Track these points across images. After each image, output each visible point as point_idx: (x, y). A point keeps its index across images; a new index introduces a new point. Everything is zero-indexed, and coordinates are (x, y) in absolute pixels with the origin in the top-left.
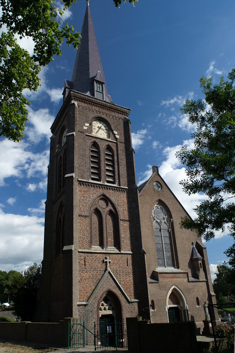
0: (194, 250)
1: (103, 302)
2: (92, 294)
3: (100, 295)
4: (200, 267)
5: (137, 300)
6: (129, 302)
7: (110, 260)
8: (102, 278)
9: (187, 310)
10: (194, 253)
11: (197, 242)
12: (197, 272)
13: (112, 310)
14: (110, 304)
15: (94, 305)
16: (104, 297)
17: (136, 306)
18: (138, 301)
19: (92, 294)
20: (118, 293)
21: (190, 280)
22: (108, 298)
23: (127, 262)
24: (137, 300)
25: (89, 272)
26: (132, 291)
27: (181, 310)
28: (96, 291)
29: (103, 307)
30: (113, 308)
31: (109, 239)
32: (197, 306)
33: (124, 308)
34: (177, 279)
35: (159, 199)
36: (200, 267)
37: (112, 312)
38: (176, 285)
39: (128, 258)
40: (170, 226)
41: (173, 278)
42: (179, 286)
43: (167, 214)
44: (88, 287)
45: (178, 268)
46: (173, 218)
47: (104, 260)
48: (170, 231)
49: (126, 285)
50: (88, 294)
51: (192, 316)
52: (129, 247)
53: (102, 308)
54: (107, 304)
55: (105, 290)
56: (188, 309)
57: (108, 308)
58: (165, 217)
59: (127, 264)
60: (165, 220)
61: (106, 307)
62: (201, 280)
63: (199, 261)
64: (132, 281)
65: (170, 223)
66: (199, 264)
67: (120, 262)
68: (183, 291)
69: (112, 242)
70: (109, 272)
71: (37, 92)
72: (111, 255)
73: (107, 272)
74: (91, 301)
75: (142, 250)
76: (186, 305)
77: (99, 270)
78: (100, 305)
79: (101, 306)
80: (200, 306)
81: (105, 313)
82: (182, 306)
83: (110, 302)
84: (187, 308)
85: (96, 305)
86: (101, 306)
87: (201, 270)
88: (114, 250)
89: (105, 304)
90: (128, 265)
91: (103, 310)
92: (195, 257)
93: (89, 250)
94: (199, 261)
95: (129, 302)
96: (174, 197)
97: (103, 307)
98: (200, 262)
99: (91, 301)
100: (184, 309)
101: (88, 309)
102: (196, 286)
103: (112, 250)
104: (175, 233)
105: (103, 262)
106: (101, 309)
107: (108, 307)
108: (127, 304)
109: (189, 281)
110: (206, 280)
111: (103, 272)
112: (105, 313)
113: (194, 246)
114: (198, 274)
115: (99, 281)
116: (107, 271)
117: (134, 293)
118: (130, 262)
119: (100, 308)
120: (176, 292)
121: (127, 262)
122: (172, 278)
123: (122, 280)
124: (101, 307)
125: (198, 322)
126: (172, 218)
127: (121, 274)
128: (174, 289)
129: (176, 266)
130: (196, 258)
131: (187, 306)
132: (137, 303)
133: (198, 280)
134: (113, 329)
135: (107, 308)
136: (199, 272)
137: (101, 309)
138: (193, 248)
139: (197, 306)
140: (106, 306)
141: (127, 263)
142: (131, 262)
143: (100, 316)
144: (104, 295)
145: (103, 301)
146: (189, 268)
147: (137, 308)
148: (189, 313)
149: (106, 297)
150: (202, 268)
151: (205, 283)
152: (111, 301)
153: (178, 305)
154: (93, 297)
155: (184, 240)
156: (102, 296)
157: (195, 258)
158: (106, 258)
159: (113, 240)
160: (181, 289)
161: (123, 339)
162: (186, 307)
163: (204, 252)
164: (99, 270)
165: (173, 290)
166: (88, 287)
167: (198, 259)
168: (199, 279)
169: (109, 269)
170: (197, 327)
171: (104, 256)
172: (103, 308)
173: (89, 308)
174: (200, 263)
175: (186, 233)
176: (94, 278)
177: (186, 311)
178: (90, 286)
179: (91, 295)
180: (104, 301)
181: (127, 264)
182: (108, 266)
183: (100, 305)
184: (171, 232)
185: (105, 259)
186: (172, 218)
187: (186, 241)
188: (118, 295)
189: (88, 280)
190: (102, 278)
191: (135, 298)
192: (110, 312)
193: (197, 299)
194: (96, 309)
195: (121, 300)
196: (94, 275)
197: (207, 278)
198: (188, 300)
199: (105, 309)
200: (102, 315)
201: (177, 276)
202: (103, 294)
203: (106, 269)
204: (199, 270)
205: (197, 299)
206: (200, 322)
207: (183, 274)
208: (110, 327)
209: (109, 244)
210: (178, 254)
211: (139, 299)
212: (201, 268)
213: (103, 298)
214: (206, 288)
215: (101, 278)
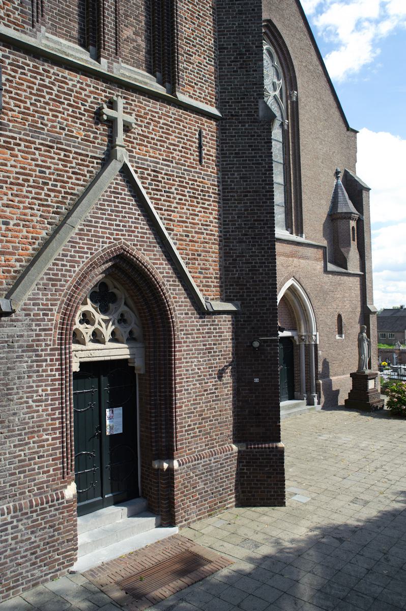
0: (340, 192)
1: (89, 307)
2: (32, 263)
3: (77, 269)
4: (351, 239)
5: (230, 307)
6: (202, 312)
7: (131, 119)
8: (91, 192)
9: (316, 345)
10: (340, 199)
11: (346, 173)
12: (342, 250)
13: (131, 339)
14: (122, 315)
15: (47, 315)
16: (94, 282)
17: (225, 325)
18: (234, 309)
19: (32, 263)
20: (161, 271)
21: (329, 269)
22: (112, 290)
23: (200, 147)
24: (230, 307)
25: (22, 148)
26: (213, 269)
27: (299, 345)
28: (57, 249)
29: (91, 329)
30: (131, 333)
31: (127, 33)
32: (338, 337)
33: (180, 335)
34: (302, 261)
35: (269, 18)
36: (351, 239)
37: (127, 351)
38: (297, 277)
39: (204, 133)
40: (289, 111)
41: (292, 257)
42: (304, 282)
43: (281, 75)
44: (11, 226)
45: (300, 232)
46: (299, 90)
47: (101, 109)
48: (286, 127)
49: (191, 241)
50: (13, 262)
51: (325, 360)
52: (209, 89)
53: (86, 331)
54: (107, 318)
55: (101, 248)
56: (318, 343)
57: (113, 333)
58: (277, 82)
59: (200, 156)
60: (277, 93)
61: (103, 330)
62: (352, 272)
63: (351, 221)
64: (214, 229)
65: (289, 101)
66: (351, 228)
67: (173, 139)
68: (311, 295)
69: (137, 49)
70: (125, 171)
71: (79, 312)
72: (134, 97)
73: (114, 167)
74: (29, 293)
75: (261, 106)
76: (314, 333)
77: (73, 150)
78: (77, 320)
79: (81, 322)
80: (343, 335)
81: (97, 353)
82: (304, 334)
83: (123, 308)
84: (316, 340)
85: (57, 317)
86: (81, 322)
87: (354, 245)
88: (148, 81)
89: (99, 317)
90: (200, 161)
91: (87, 339)
92: (341, 209)
93: (23, 35)
94: (351, 221)
95: (202, 312)
96: (305, 29)
97: (91, 329)
98: (353, 224)
99: (29, 293)
100: (307, 343)
101: (12, 336)
102: (340, 285)
103: (140, 78)
104: (301, 134)
105: (98, 116)
106: (77, 338)
107: (111, 328)
108: (194, 321)
109: (326, 271)
110: (362, 273)
111: (95, 166)
112: (97, 353)
113: (340, 181)
114: (346, 255)
115: (76, 206)
116: (113, 163)
117: (220, 278)
118: (211, 149)
119: (75, 334)
120: (293, 298)
121: (200, 147)
122: (288, 257)
123: (175, 216)
124: (78, 326)
125: (335, 375)
126: (297, 90)
127: (173, 190)
128: (292, 286)
129: (294, 227)
130: (346, 213)
131: (317, 336)
132: (229, 317)
133: (344, 270)
134: (128, 420)
135: (107, 333)
136: (349, 250)
137: (77, 338)
138: (337, 185)
139: (337, 336)
140: (103, 324)
141: (200, 152)
142: (213, 152)
143: (76, 368)
144: (97, 276)
145: (88, 300)
146: (324, 236)
147: (228, 335)
148: (320, 353)
149: (102, 285)
150: (356, 240)
151: (356, 281)
152: (126, 304)
153: (295, 333)
154: (39, 275)
155: (317, 158)
156: (86, 280)
157: (342, 213)
158: (112, 105)
159: (141, 42)
160: (308, 291)
161: (173, 459)
162: (314, 337)
163: (364, 199)
164: (73, 150)
165: (289, 293)
166: (11, 226)
167: (348, 216)
168: (346, 269)
169: (122, 154)
170: (334, 389)
171: (103, 91)
172: (90, 333)
173: (18, 329)
174: (353, 227)
175: (324, 141)
176: (47, 184)
177: (312, 349)
178: (26, 223)
179: (28, 269)
180: (91, 300)
181: (200, 156)
182: (121, 137)
183: (77, 320)
184: (290, 131)
185: (105, 106)
186: (297, 90)
187: (322, 163)
188: (159, 277)
189: (15, 187)
190: (88, 190)
191: (227, 300)
192: (120, 351)
193: (340, 317)
194: (55, 334)
195: (171, 300)
196: (48, 171)
197: (363, 267)
198: (321, 319)
199: (97, 337)
200: (83, 365)
201: (300, 254)
202: (92, 266)
203: (110, 155)
204: (349, 245)
205: (340, 317)
206: (339, 377)
207: (315, 250)
208: (119, 411)
209: (125, 49)
210: (304, 196)
211: (239, 303)
212: (354, 240)
213: (90, 285)
214: (359, 292)
215: (85, 194)
